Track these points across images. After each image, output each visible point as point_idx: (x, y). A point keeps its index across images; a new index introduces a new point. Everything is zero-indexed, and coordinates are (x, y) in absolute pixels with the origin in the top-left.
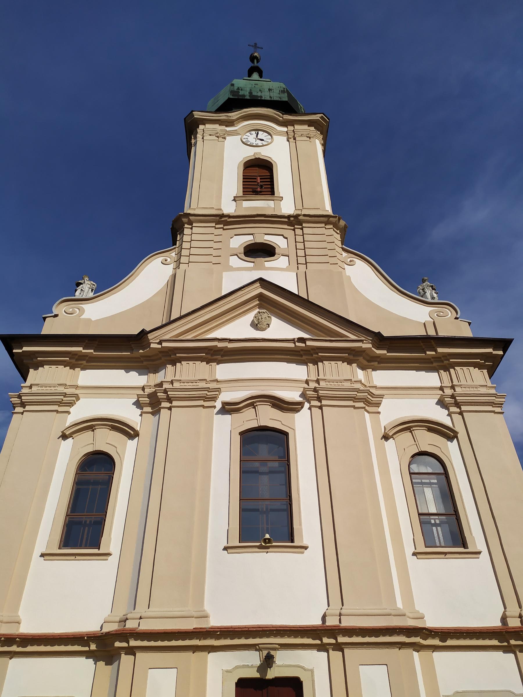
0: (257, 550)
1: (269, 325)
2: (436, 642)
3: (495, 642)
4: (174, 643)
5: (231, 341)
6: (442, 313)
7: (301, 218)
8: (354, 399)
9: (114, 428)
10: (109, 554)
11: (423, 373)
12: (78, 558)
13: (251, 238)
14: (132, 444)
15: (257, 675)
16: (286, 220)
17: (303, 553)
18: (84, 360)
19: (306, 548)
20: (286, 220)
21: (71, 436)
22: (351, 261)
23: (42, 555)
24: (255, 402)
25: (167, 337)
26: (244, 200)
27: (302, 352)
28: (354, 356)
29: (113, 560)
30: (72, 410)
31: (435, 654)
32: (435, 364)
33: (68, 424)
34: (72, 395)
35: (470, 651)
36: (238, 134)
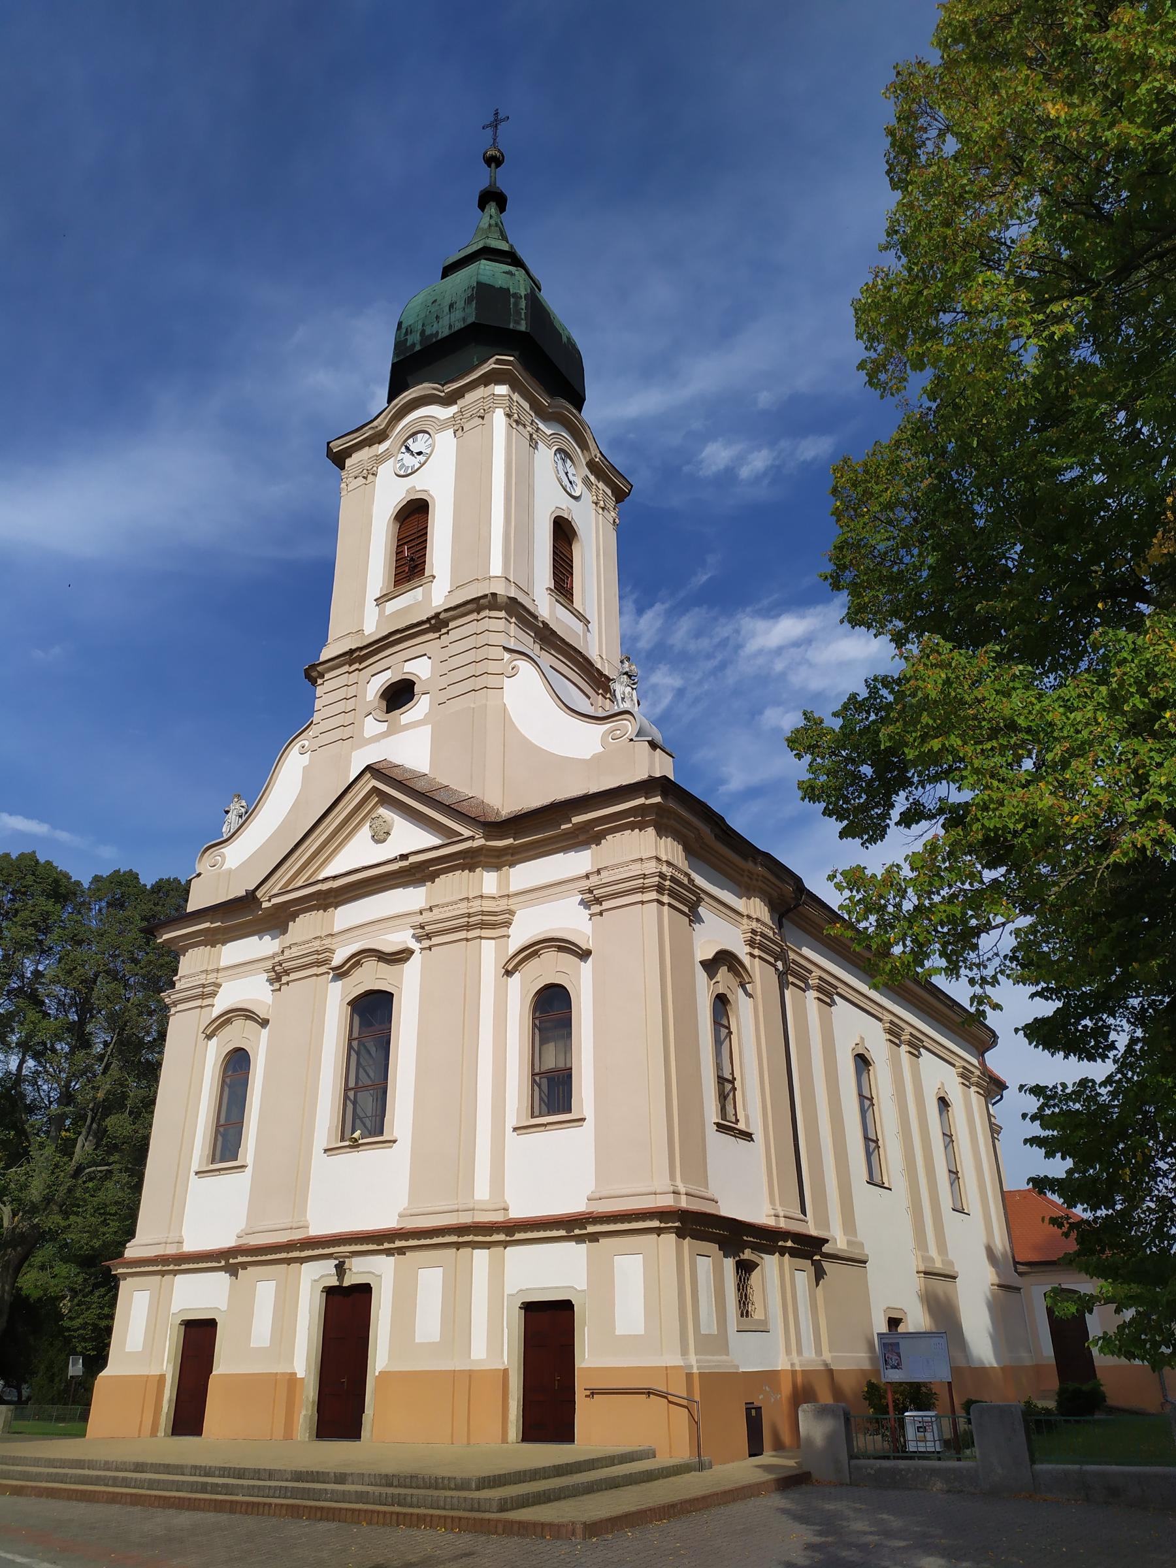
0: (349, 1150)
1: (388, 834)
2: (501, 1237)
3: (562, 1233)
4: (435, 1241)
5: (335, 878)
6: (618, 732)
7: (442, 616)
8: (468, 927)
9: (561, 949)
10: (583, 1120)
11: (572, 854)
12: (222, 1172)
13: (388, 674)
14: (586, 968)
15: (337, 1284)
16: (428, 626)
17: (391, 1147)
18: (506, 854)
19: (395, 1141)
20: (428, 626)
21: (515, 969)
22: (513, 669)
23: (515, 1129)
24: (361, 960)
25: (275, 891)
26: (386, 601)
27: (413, 871)
28: (472, 858)
29: (589, 1124)
30: (511, 931)
31: (476, 1252)
32: (581, 838)
33: (511, 951)
34: (502, 912)
35: (551, 1242)
36: (391, 456)
